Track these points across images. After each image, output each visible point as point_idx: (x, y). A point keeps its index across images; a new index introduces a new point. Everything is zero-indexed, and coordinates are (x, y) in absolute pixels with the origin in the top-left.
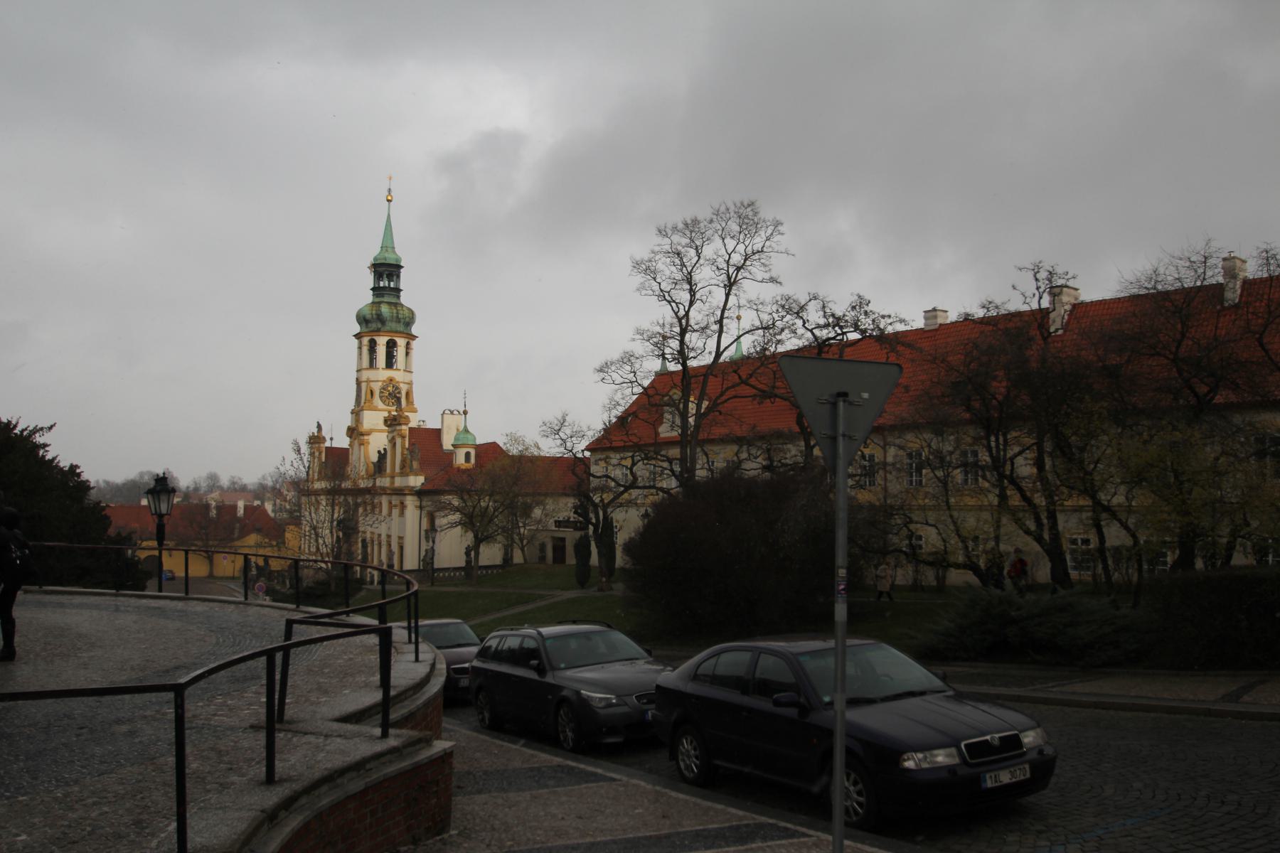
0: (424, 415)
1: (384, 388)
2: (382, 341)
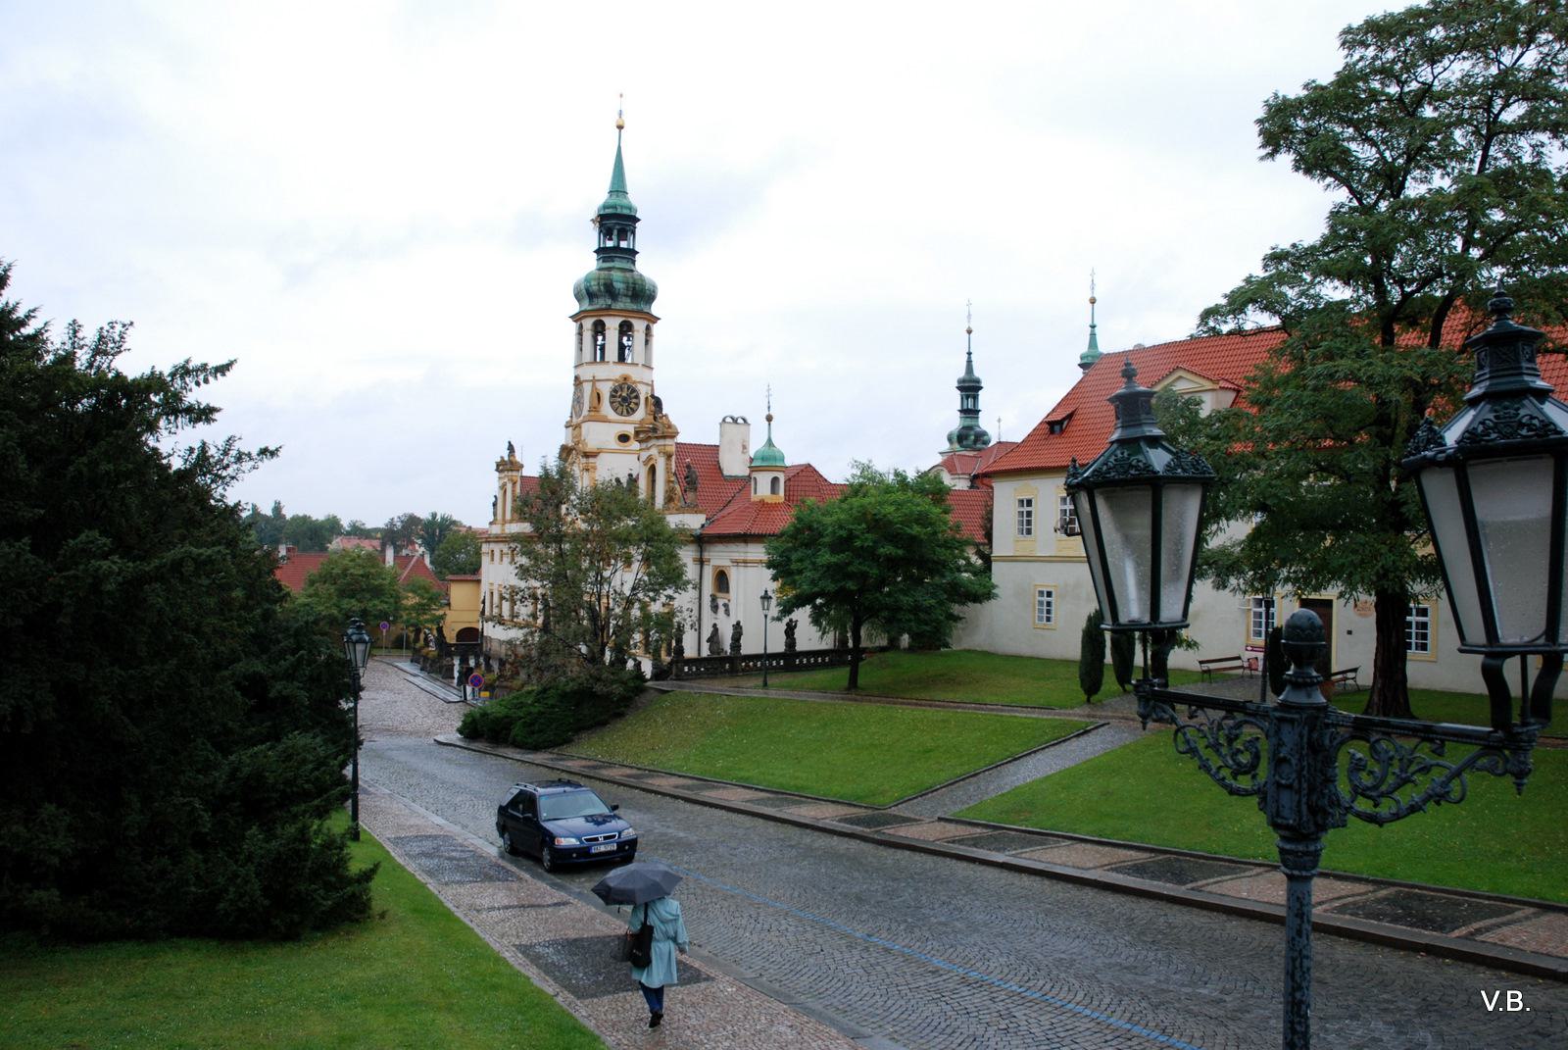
2: (612, 324)
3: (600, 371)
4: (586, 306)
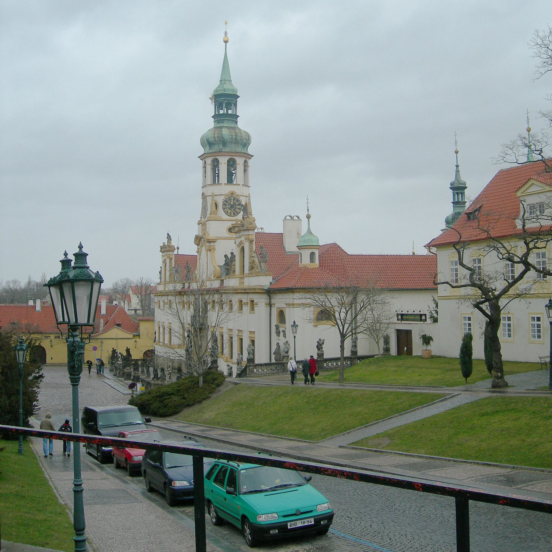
0: (267, 221)
1: (225, 203)
2: (223, 161)
3: (216, 190)
4: (208, 150)
